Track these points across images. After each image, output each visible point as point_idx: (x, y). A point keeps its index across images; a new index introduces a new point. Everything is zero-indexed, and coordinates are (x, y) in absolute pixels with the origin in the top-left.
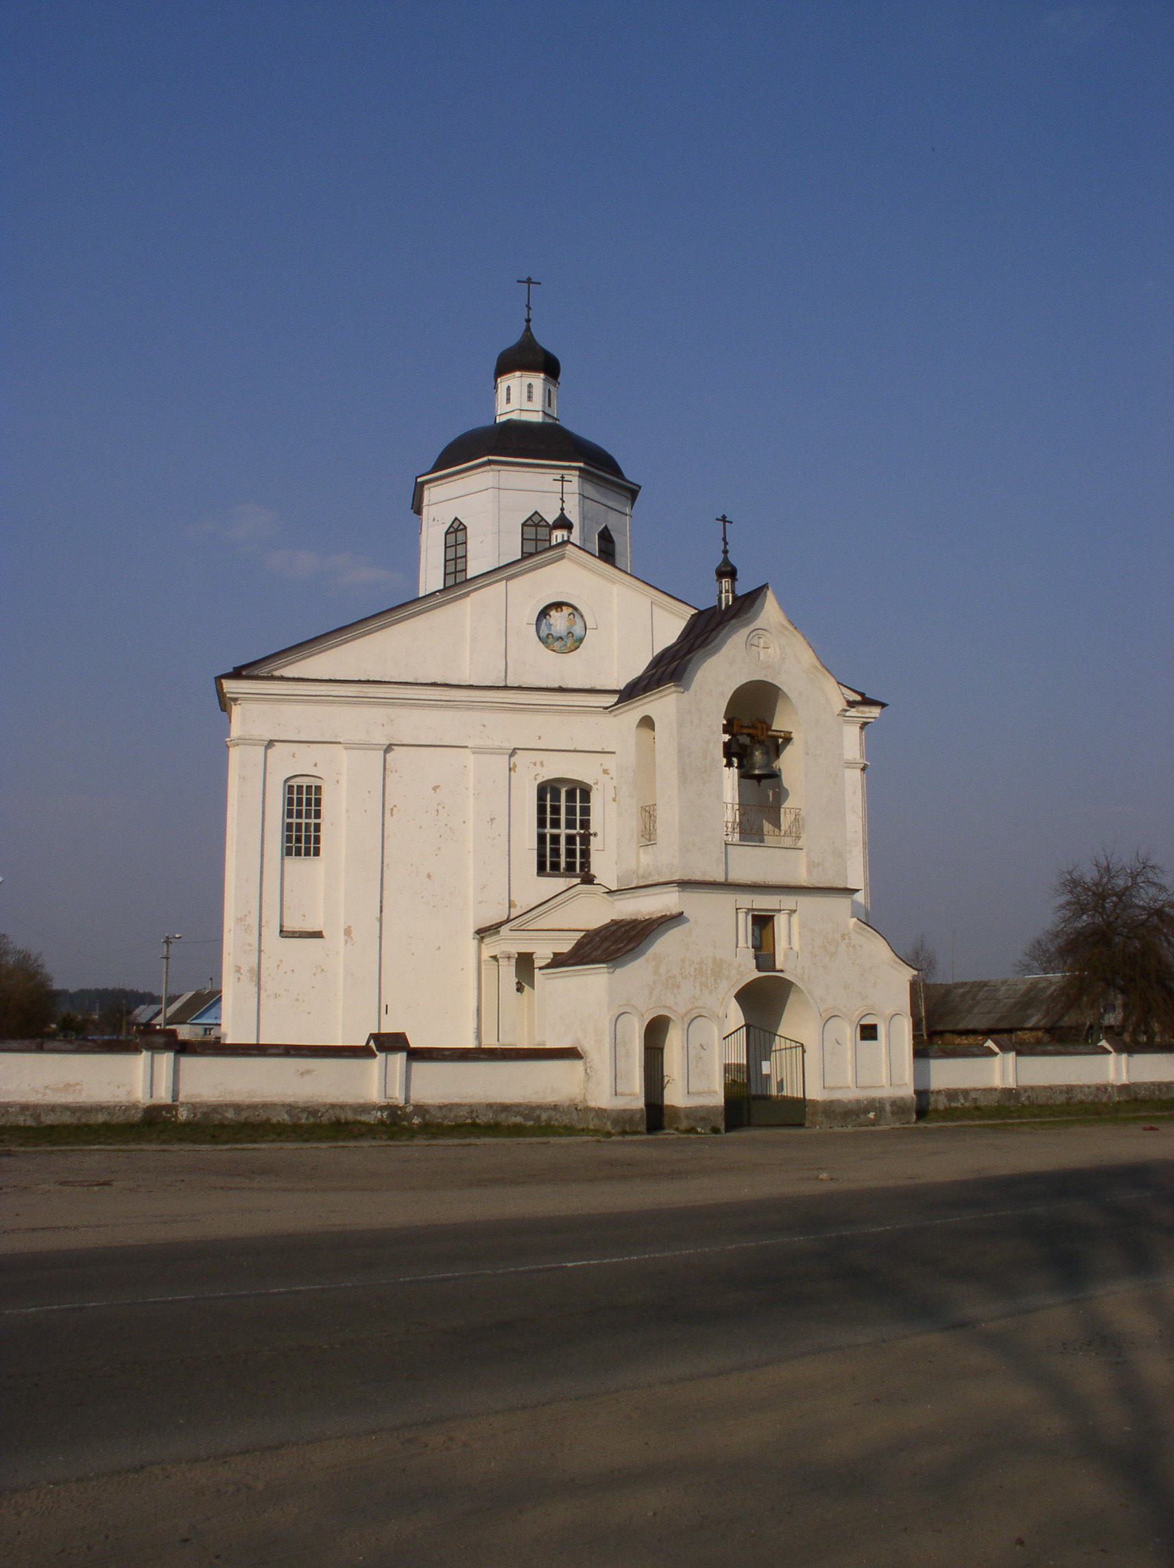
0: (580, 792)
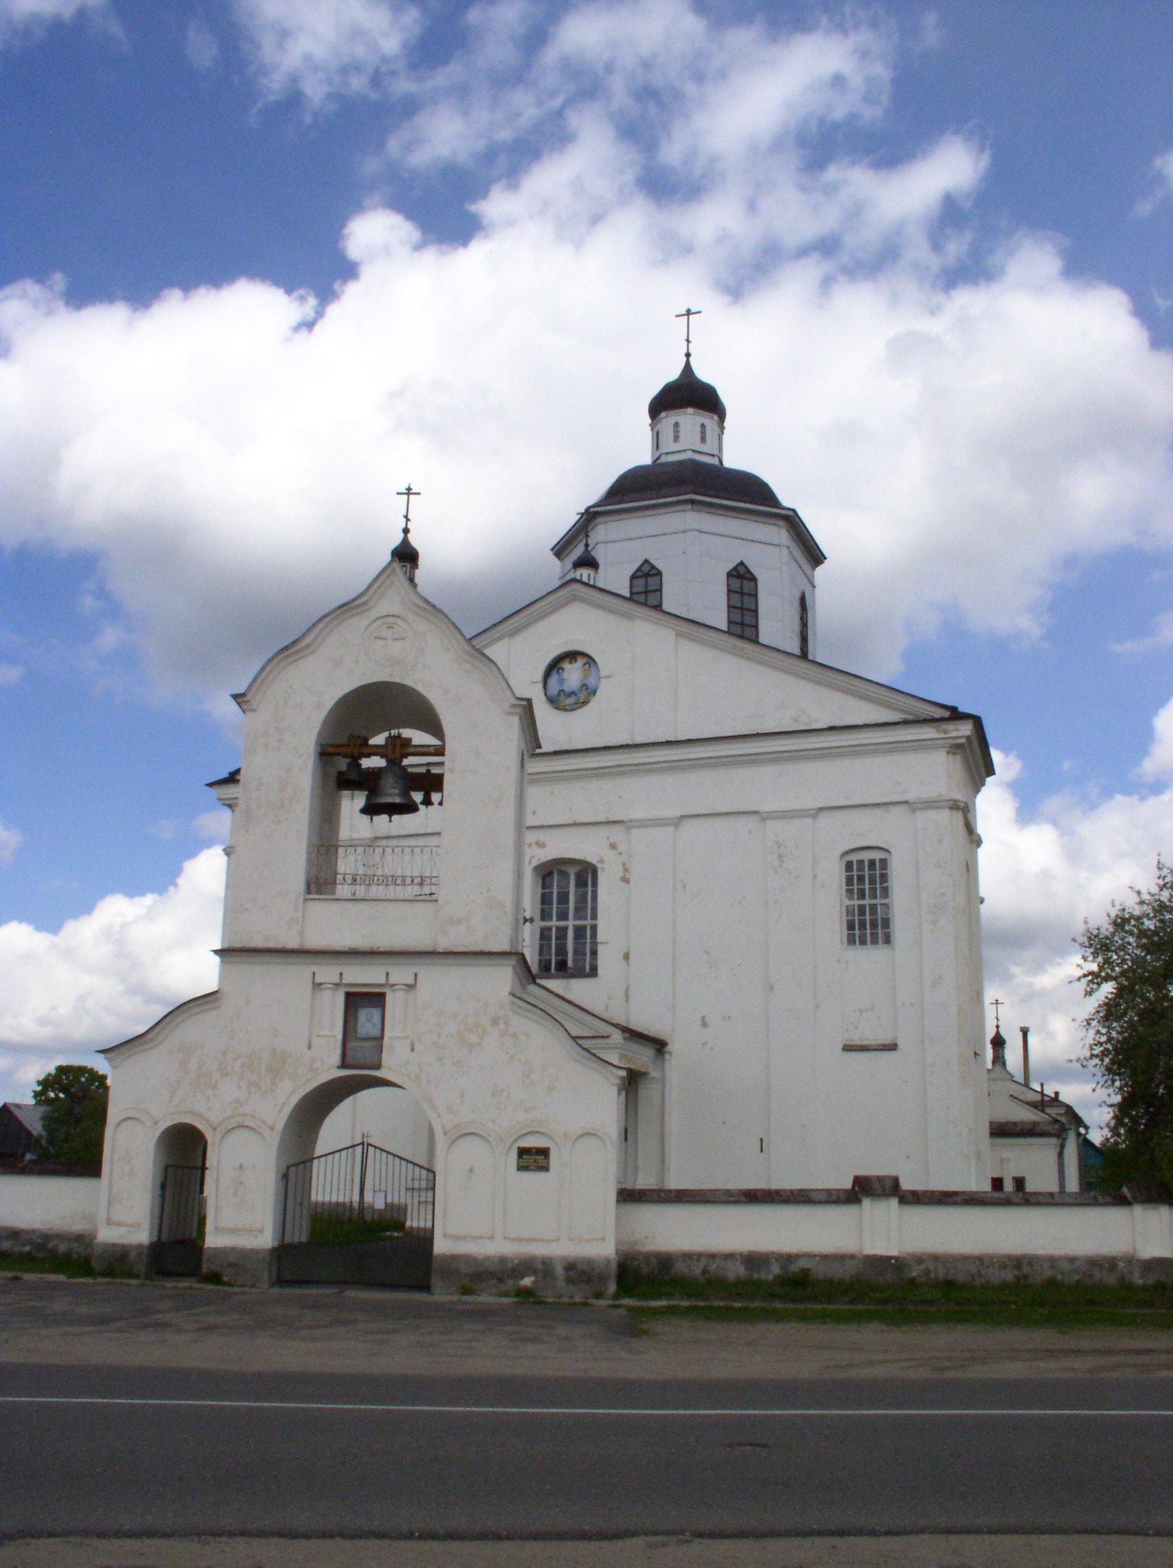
0: (586, 874)
